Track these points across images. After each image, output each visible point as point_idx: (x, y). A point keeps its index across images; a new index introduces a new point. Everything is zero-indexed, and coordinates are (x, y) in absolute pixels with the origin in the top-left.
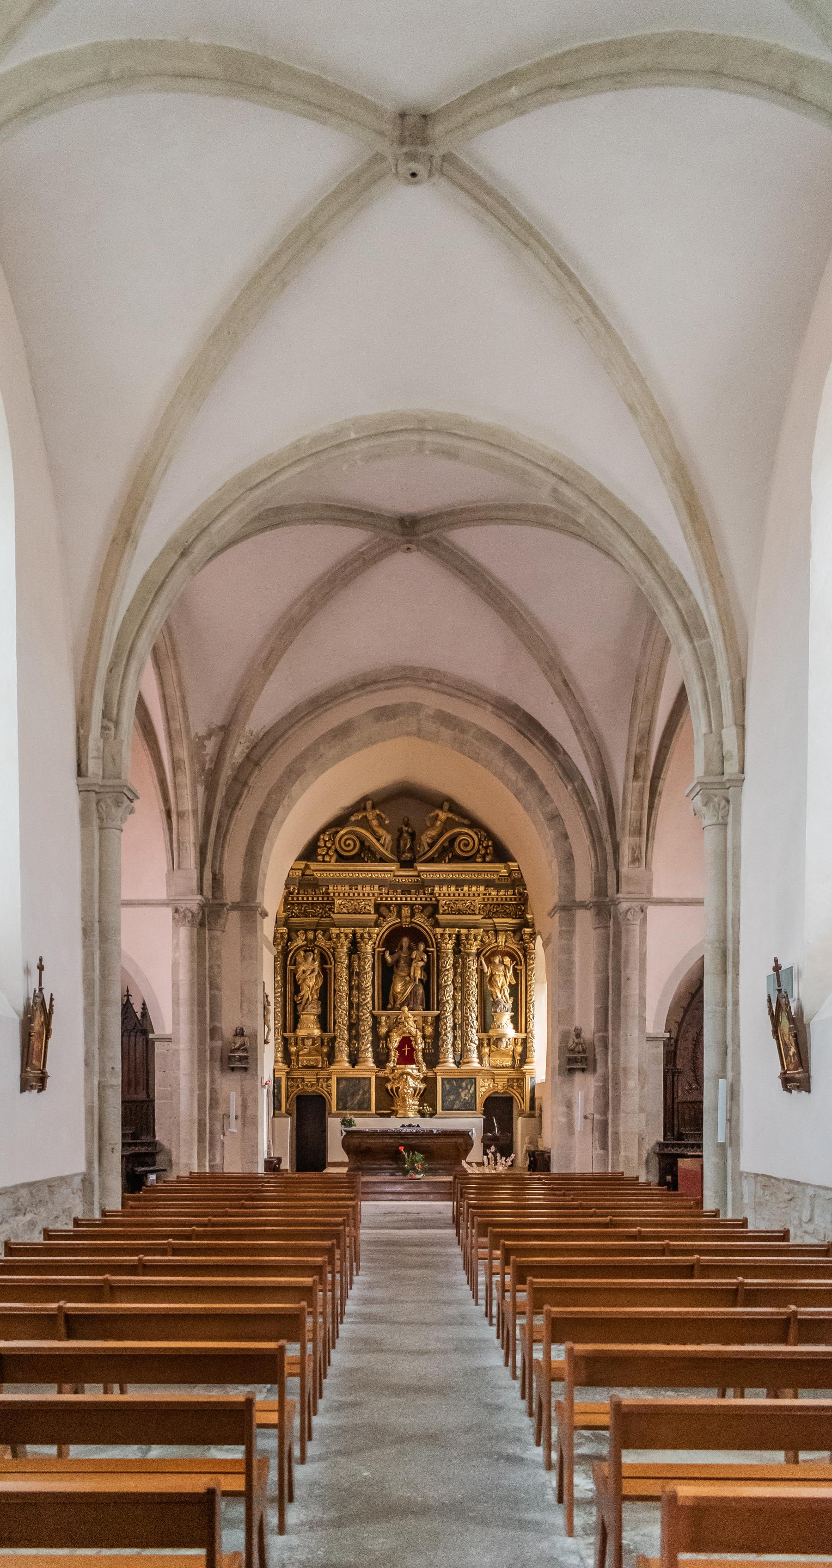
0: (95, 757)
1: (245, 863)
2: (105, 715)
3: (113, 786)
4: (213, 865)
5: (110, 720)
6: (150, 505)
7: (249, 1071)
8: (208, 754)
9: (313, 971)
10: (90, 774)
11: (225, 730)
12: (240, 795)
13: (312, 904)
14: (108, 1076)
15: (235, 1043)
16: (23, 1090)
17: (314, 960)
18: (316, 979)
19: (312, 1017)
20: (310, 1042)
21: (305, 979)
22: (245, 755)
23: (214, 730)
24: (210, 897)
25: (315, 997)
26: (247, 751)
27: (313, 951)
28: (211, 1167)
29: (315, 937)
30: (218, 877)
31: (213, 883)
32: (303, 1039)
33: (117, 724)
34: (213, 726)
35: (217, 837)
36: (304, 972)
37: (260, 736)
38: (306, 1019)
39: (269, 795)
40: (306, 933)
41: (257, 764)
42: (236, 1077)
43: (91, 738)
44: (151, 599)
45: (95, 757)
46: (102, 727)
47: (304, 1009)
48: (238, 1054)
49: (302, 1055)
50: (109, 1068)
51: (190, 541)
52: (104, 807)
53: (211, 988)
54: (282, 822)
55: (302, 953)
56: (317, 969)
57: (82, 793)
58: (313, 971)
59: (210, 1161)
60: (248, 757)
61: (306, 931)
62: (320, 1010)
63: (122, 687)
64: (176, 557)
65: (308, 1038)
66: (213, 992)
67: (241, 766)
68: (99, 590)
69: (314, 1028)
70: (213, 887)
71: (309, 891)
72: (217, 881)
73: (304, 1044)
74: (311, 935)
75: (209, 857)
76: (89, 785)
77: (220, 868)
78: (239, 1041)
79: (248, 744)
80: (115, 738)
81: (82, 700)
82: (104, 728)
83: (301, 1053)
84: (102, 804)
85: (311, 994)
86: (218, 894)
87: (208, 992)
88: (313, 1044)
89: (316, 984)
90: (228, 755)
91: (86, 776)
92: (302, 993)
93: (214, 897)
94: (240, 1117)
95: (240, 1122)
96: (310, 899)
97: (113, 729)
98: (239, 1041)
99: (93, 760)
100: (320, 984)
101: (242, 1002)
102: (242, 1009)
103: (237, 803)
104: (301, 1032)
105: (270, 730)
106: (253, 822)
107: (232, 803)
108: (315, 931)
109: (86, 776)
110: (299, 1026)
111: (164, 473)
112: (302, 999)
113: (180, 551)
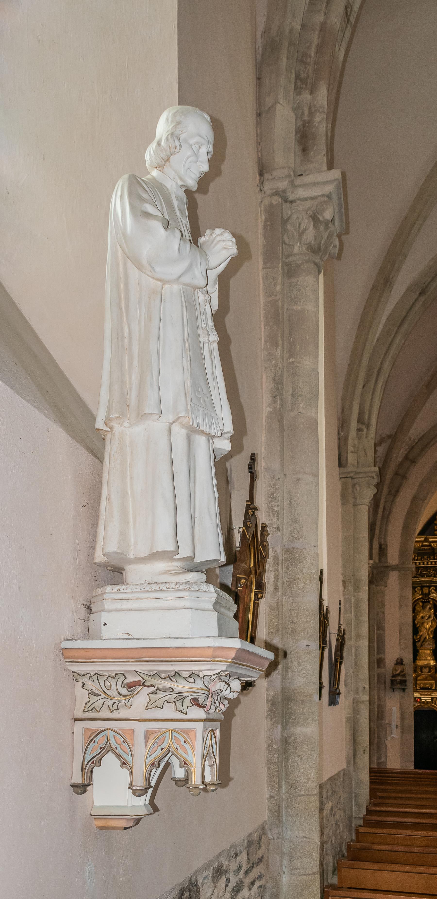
0: (352, 452)
1: (402, 536)
2: (360, 420)
3: (366, 473)
4: (379, 538)
5: (363, 423)
6: (406, 256)
7: (406, 691)
8: (378, 457)
9: (429, 617)
10: (349, 465)
11: (393, 439)
12: (401, 485)
13: (427, 567)
14: (361, 694)
15: (396, 670)
16: (329, 705)
17: (430, 609)
18: (431, 623)
19: (429, 652)
20: (427, 670)
21: (423, 623)
22: (404, 455)
23: (383, 438)
24: (377, 561)
25: (431, 636)
26: (406, 452)
27: (429, 602)
28: (378, 763)
29: (429, 592)
30: (383, 547)
31: (379, 551)
32: (421, 668)
33: (368, 426)
34: (384, 436)
35: (383, 516)
36: (422, 618)
37: (416, 441)
38: (424, 653)
39: (421, 484)
40: (422, 589)
41: (414, 462)
42: (397, 695)
43: (350, 437)
44: (395, 331)
45: (352, 452)
46: (357, 429)
47: (422, 646)
48: (399, 678)
49: (420, 680)
50: (361, 689)
51: (426, 283)
52: (358, 489)
53: (378, 629)
54: (427, 504)
55: (421, 604)
56: (433, 616)
57: (342, 479)
58: (429, 617)
59: (378, 759)
60: (406, 457)
61: (422, 587)
62: (434, 646)
63: (372, 398)
64: (415, 296)
65: (425, 667)
66: (379, 632)
67: (401, 464)
68: (359, 326)
69: (430, 660)
70: (379, 554)
71: (426, 557)
72: (382, 550)
73: (422, 672)
74: (426, 590)
75: (377, 532)
76: (348, 473)
77: (385, 541)
78: (399, 669)
79: (407, 447)
80: (366, 437)
81: (343, 411)
82: (359, 430)
83: (419, 678)
84: (357, 487)
85: (428, 634)
86: (383, 560)
87: (376, 632)
88: (429, 672)
89: (431, 627)
90: (394, 456)
91: (345, 466)
92: (421, 634)
93: (380, 561)
94: (399, 726)
95: (399, 730)
96: (425, 563)
97: (365, 430)
98: (399, 669)
99: (351, 454)
100: (435, 627)
101: (400, 640)
102: (400, 645)
103: (398, 491)
104: (421, 663)
105: (423, 436)
106: (408, 505)
107: (394, 493)
108: (429, 587)
109: (345, 466)
110: (418, 658)
111: (419, 231)
112: (420, 638)
113: (418, 292)
